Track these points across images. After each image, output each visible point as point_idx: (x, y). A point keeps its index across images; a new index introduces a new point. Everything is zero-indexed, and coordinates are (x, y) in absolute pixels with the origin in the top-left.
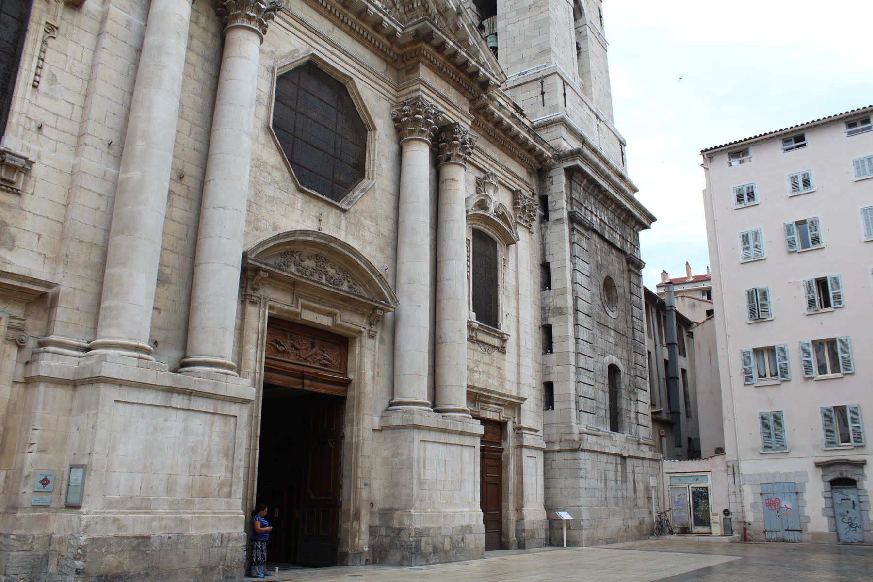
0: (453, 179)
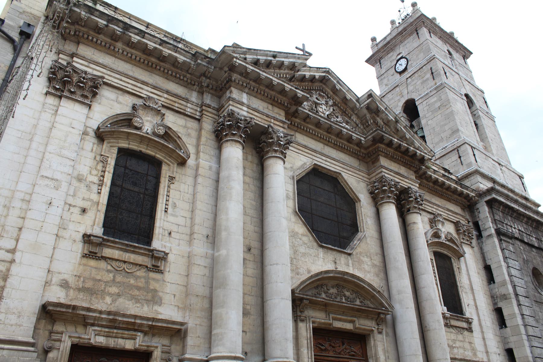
0: (414, 223)
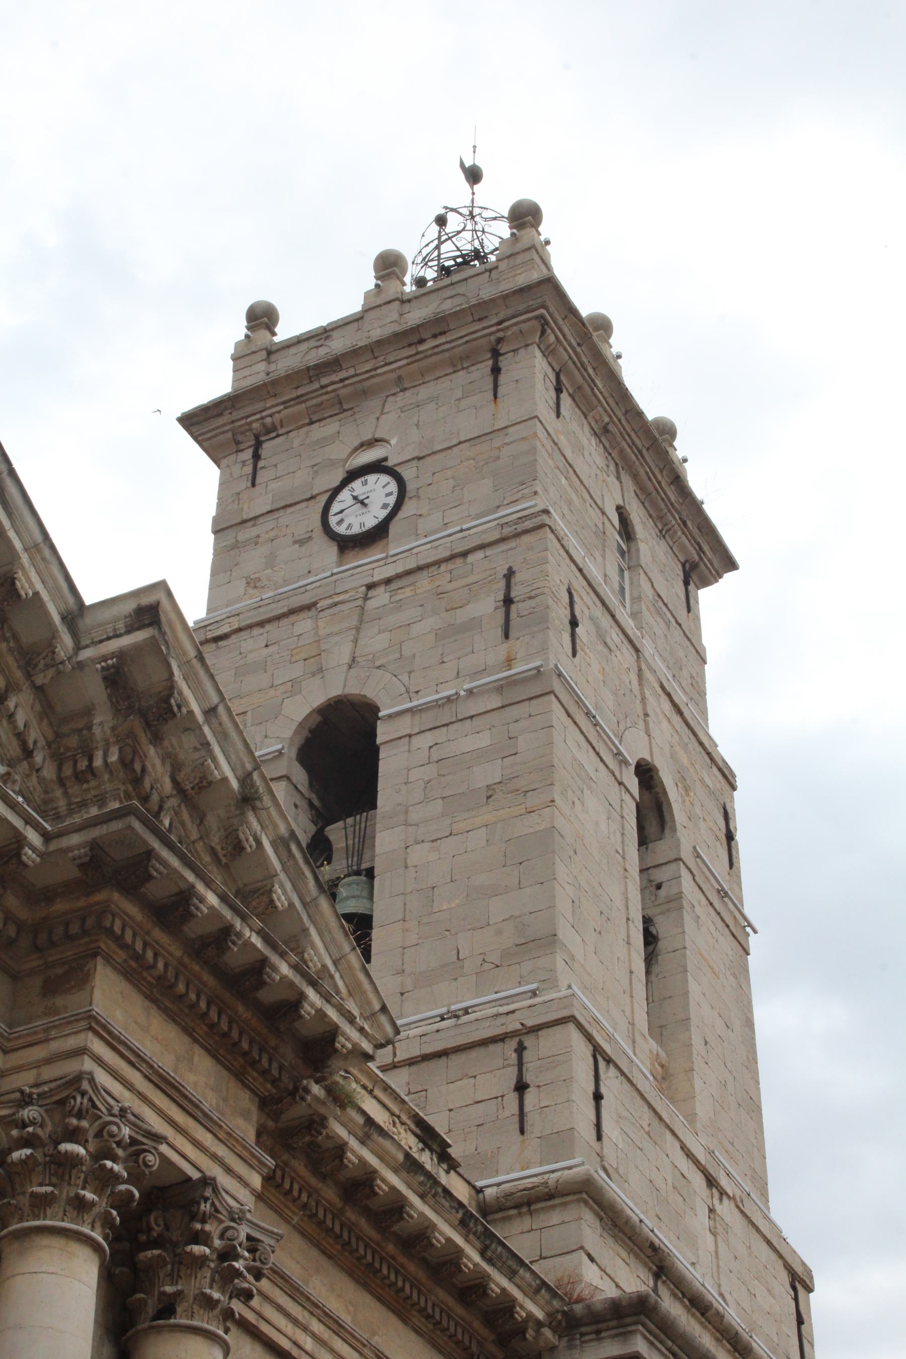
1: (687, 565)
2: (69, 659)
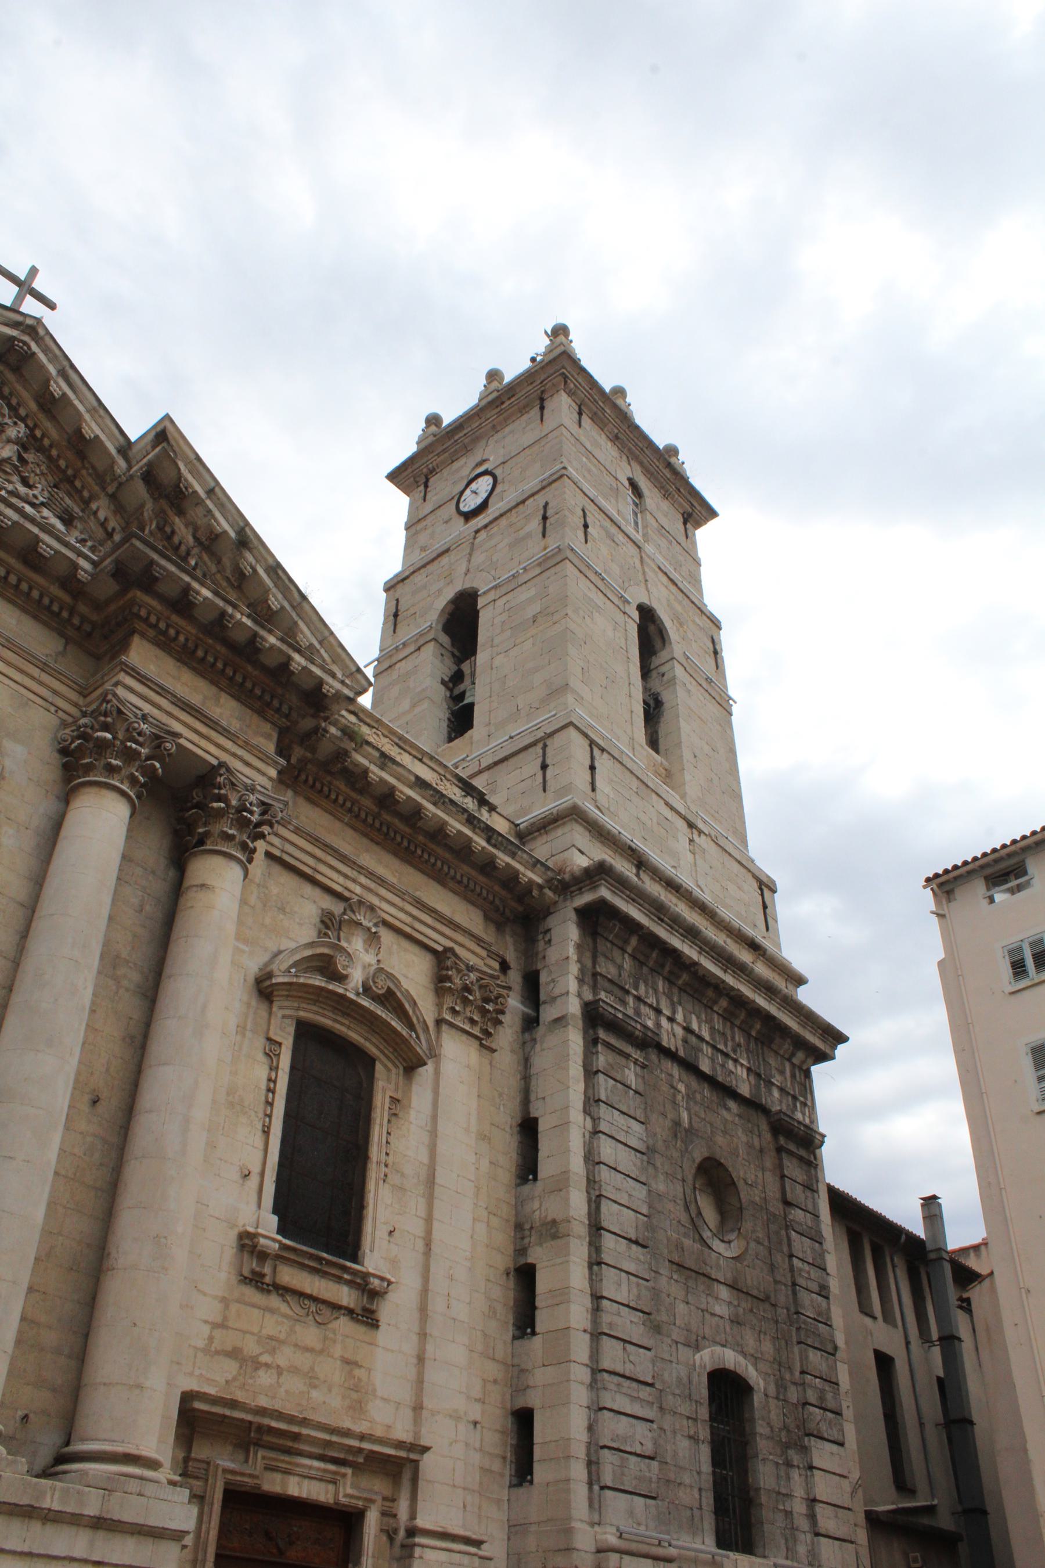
0: (203, 885)
1: (685, 516)
2: (124, 474)
